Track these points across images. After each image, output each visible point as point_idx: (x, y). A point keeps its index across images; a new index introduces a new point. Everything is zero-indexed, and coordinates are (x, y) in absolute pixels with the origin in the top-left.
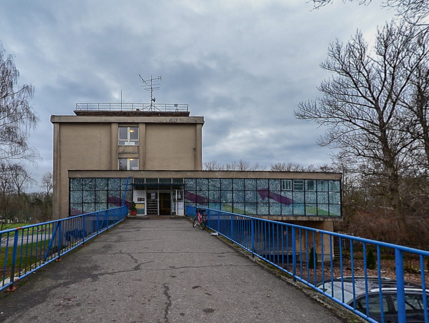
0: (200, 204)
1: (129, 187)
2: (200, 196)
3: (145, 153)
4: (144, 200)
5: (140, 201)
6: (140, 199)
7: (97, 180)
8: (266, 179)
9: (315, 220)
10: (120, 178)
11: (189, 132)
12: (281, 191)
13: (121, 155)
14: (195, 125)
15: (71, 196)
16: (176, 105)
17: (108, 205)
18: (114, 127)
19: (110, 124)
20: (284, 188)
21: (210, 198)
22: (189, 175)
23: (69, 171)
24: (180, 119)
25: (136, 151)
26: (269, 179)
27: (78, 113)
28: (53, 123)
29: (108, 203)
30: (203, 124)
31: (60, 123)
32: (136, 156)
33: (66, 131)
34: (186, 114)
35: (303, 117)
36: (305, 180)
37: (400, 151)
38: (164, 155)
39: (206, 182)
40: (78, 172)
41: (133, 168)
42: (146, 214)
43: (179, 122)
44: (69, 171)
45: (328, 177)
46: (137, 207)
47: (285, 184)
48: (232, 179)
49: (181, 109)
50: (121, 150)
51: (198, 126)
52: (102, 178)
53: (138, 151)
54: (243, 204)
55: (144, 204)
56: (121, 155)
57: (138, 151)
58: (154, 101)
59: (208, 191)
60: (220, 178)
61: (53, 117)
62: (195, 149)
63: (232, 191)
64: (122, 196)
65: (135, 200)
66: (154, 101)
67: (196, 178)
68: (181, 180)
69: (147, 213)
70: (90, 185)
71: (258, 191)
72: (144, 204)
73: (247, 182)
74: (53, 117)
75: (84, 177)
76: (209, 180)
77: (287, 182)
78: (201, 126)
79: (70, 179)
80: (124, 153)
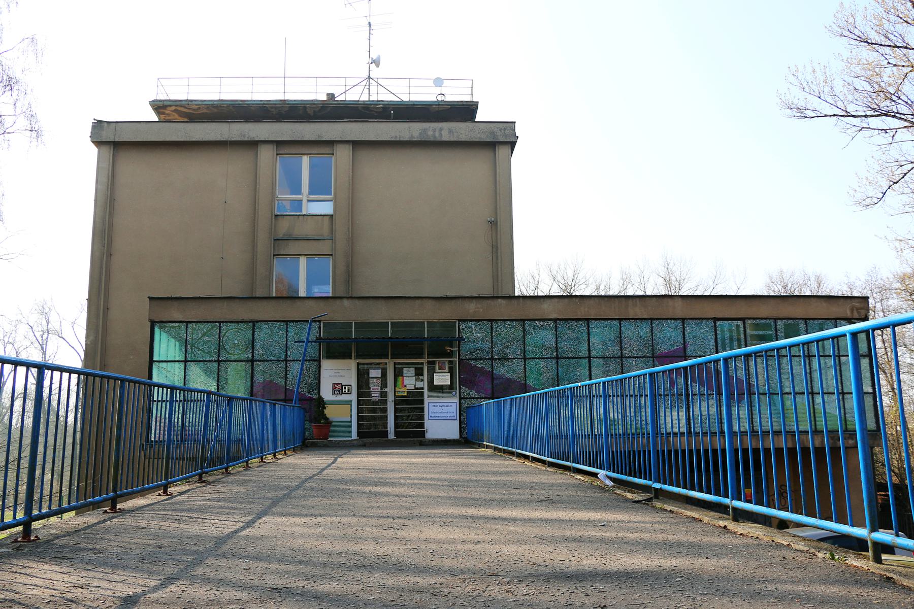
1: (312, 350)
3: (352, 240)
5: (341, 393)
6: (338, 389)
8: (708, 319)
13: (281, 243)
16: (438, 82)
18: (266, 154)
19: (253, 145)
22: (472, 308)
24: (450, 131)
25: (326, 231)
26: (683, 320)
28: (98, 143)
30: (513, 145)
31: (114, 142)
32: (325, 247)
33: (135, 168)
34: (466, 111)
35: (801, 112)
36: (776, 319)
38: (408, 267)
39: (514, 331)
40: (175, 303)
41: (317, 291)
42: (354, 435)
43: (446, 137)
44: (150, 298)
46: (331, 412)
48: (588, 320)
49: (455, 94)
50: (283, 228)
51: (502, 151)
52: (238, 322)
53: (332, 231)
56: (281, 243)
57: (332, 231)
58: (378, 66)
59: (525, 359)
60: (555, 320)
61: (98, 125)
62: (493, 223)
63: (589, 358)
65: (326, 393)
66: (378, 66)
67: (491, 321)
68: (448, 325)
69: (359, 434)
70: (205, 343)
71: (657, 357)
73: (629, 331)
74: (98, 125)
75: (190, 318)
76: (527, 327)
78: (507, 149)
79: (153, 324)
80: (289, 238)
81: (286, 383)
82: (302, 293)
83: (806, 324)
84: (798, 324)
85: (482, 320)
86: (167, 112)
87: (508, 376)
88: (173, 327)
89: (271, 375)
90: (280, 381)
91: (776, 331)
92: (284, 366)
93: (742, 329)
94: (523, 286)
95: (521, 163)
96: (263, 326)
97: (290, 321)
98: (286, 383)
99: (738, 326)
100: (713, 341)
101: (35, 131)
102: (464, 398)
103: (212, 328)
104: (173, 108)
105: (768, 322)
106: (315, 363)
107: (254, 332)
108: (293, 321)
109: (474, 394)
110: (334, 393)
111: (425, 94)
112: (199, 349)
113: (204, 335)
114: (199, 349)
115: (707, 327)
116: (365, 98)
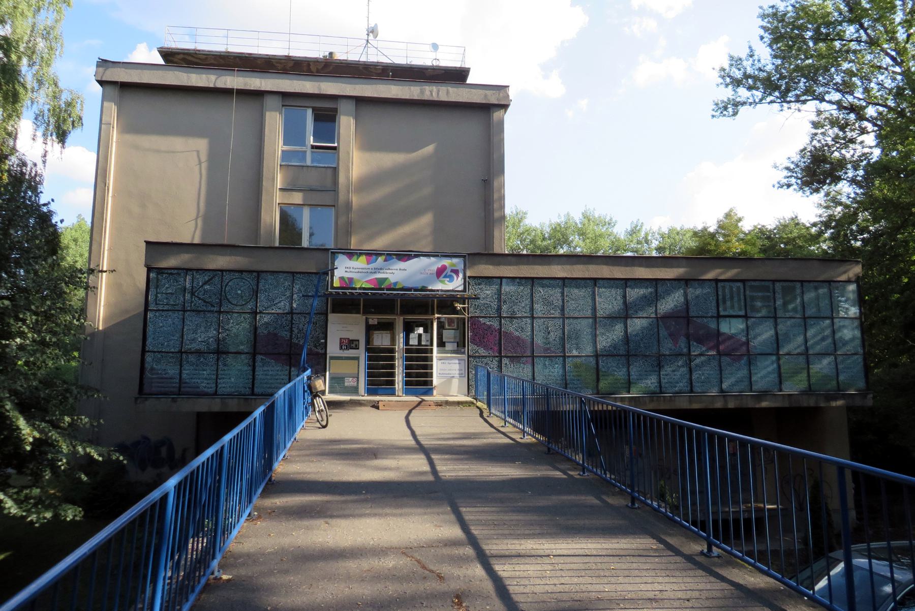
0: (512, 361)
2: (508, 335)
4: (357, 348)
7: (227, 277)
9: (805, 405)
10: (293, 273)
11: (469, 127)
12: (719, 316)
14: (486, 109)
15: (150, 328)
17: (254, 361)
19: (259, 94)
20: (725, 310)
21: (539, 340)
23: (148, 243)
27: (171, 57)
28: (101, 83)
29: (254, 355)
34: (458, 76)
36: (774, 281)
37: (822, 100)
44: (148, 243)
45: (605, 271)
47: (720, 297)
49: (448, 60)
51: (496, 115)
54: (623, 359)
55: (357, 359)
64: (296, 331)
70: (206, 291)
72: (357, 359)
74: (103, 63)
75: (808, 278)
77: (731, 288)
81: (291, 336)
82: (305, 243)
83: (802, 286)
84: (312, 161)
85: (168, 152)
86: (175, 60)
87: (517, 334)
88: (171, 274)
89: (276, 328)
90: (285, 334)
91: (774, 293)
92: (289, 318)
93: (742, 291)
94: (201, 145)
95: (513, 124)
96: (269, 276)
97: (297, 273)
98: (291, 336)
99: (738, 288)
100: (714, 302)
101: (713, 116)
102: (472, 356)
103: (214, 277)
104: (181, 56)
105: (767, 284)
106: (323, 317)
107: (258, 282)
108: (300, 273)
109: (482, 352)
110: (341, 348)
111: (424, 59)
112: (200, 299)
113: (205, 283)
114: (200, 299)
115: (709, 288)
116: (363, 59)
